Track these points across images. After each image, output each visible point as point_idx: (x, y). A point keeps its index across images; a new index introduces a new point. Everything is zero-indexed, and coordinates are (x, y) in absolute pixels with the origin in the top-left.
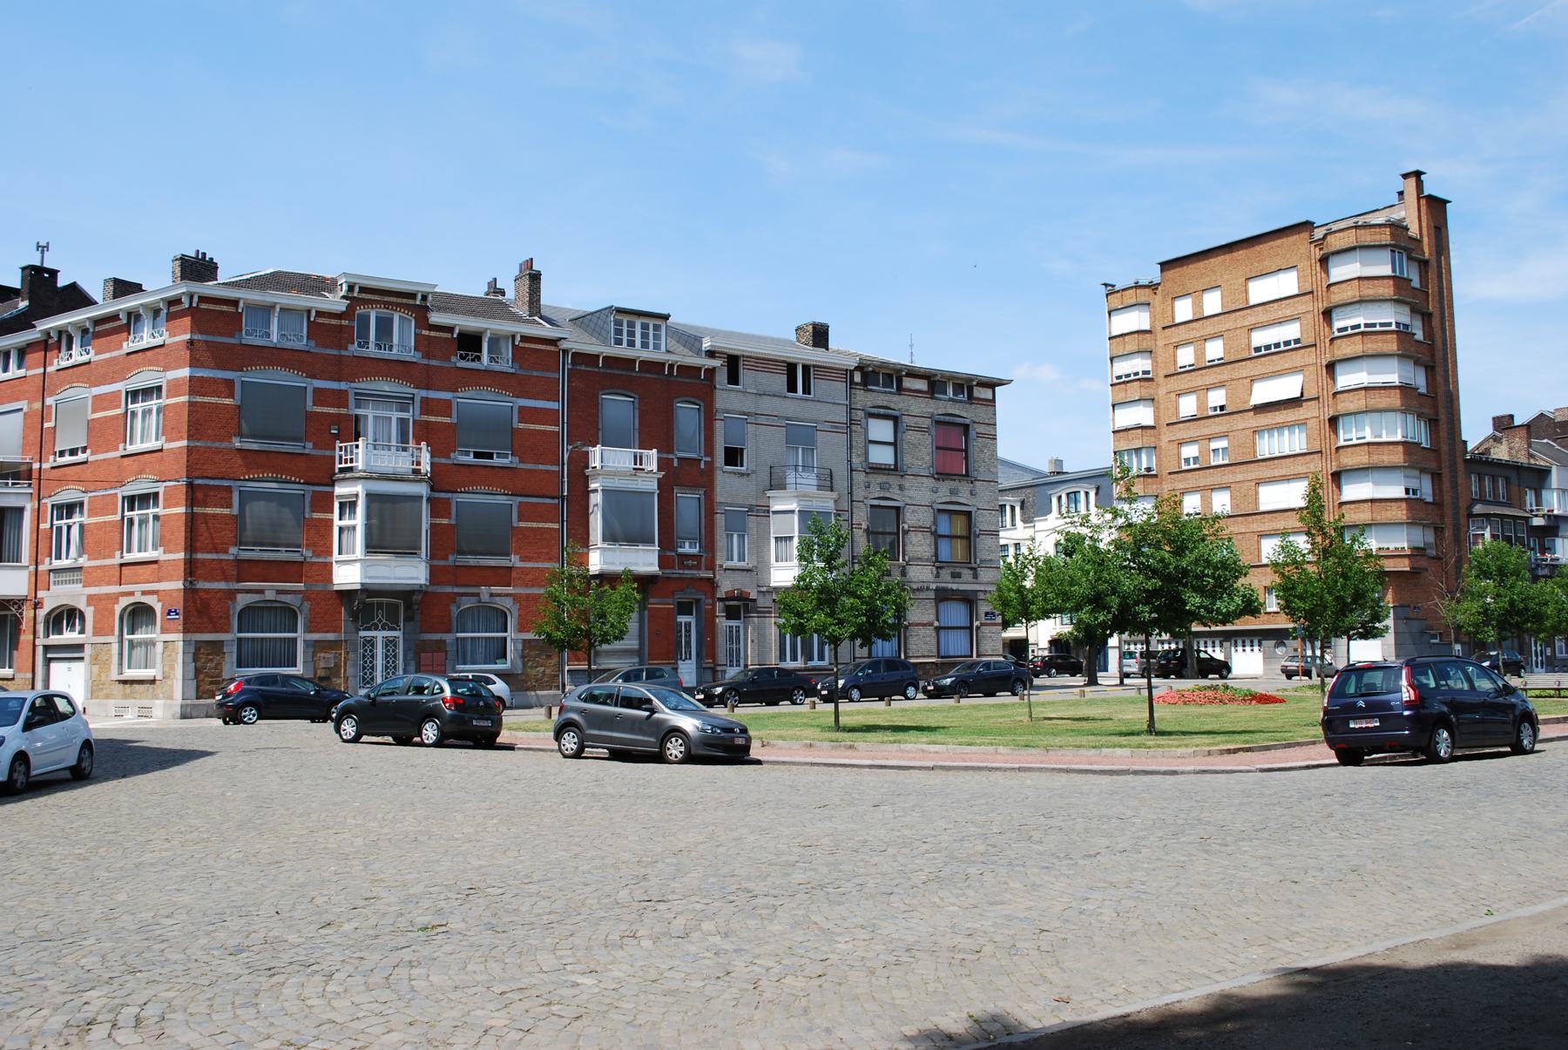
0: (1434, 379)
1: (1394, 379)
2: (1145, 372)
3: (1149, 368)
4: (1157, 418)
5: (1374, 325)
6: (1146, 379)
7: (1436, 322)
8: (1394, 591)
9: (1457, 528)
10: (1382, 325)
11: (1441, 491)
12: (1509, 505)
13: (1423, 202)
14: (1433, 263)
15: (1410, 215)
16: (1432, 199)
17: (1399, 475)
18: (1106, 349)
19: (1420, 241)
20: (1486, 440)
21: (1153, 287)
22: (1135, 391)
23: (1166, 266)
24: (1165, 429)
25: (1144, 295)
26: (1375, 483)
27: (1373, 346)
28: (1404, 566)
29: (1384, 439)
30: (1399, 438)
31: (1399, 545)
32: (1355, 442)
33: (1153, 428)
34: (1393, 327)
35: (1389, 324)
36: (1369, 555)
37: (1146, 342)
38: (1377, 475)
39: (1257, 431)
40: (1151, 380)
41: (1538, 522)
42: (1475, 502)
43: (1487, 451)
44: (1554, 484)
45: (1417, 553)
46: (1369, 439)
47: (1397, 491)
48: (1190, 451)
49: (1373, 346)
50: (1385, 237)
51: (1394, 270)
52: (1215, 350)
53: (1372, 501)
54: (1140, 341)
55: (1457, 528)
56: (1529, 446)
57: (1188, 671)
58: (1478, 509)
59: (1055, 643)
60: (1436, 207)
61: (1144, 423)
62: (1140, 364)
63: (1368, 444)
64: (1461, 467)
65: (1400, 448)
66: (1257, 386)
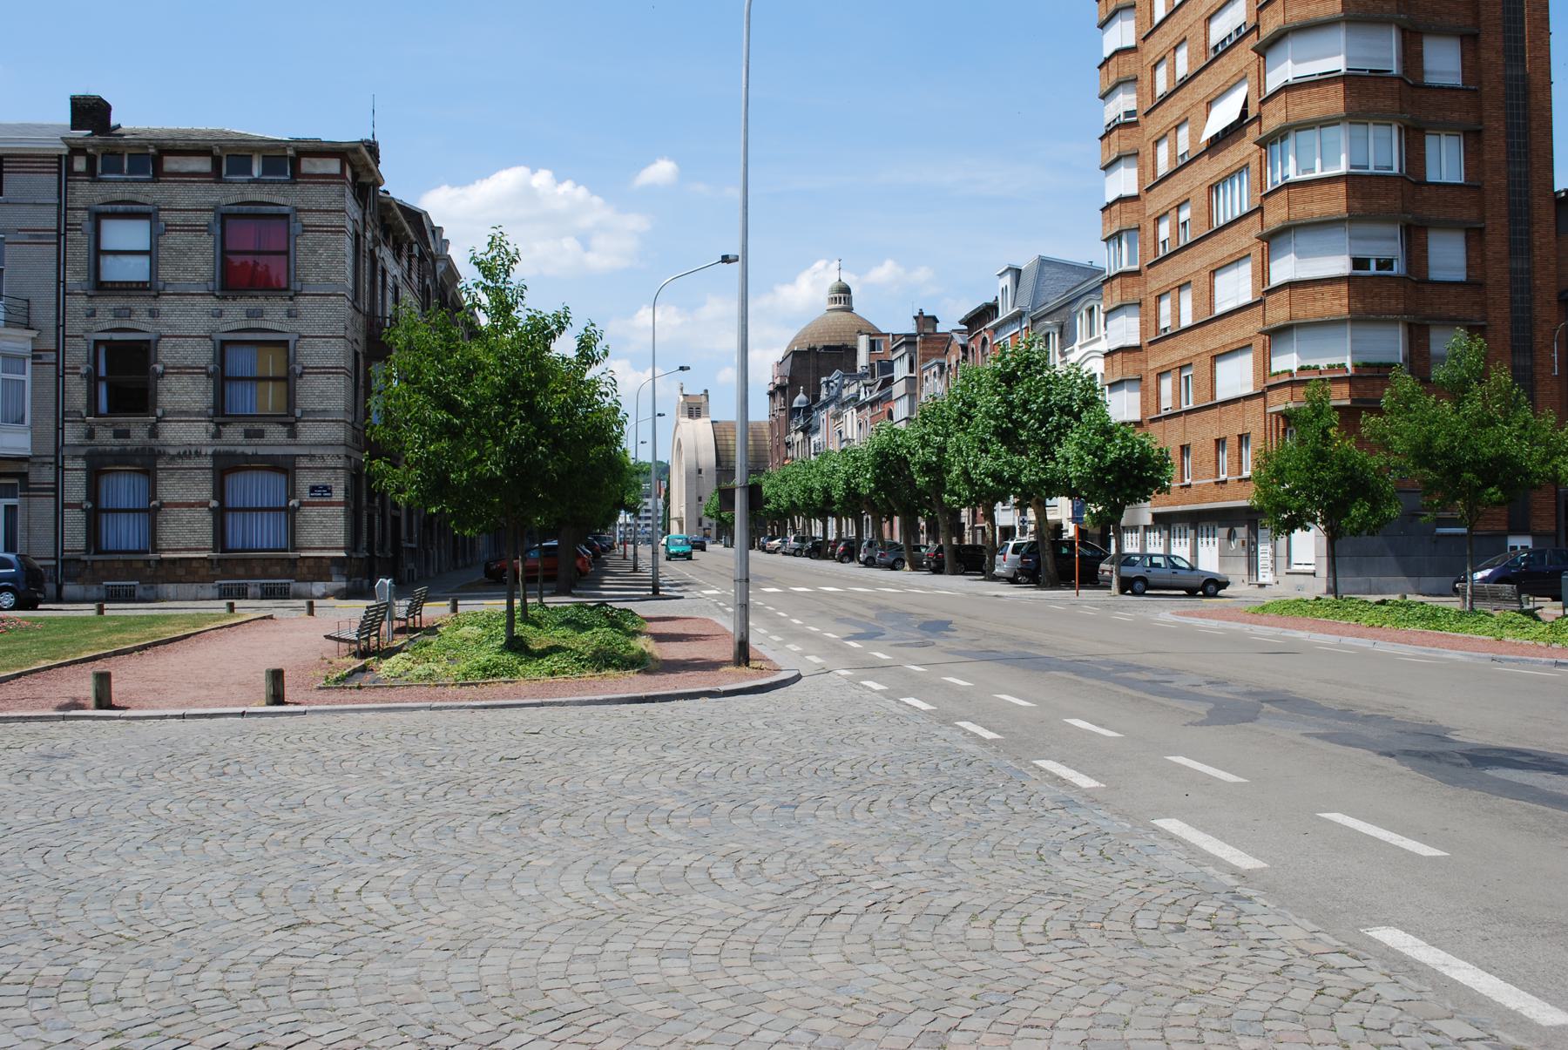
1: (1338, 63)
2: (1128, 114)
3: (1132, 107)
6: (1128, 123)
17: (1341, 237)
18: (1096, 82)
22: (1118, 143)
26: (1301, 255)
29: (1318, 173)
30: (1343, 168)
31: (1335, 361)
37: (1128, 66)
38: (1301, 240)
39: (1214, 187)
40: (1135, 124)
45: (1370, 375)
47: (1339, 265)
48: (1165, 230)
54: (1120, 71)
62: (1124, 102)
63: (1289, 186)
64: (1544, 214)
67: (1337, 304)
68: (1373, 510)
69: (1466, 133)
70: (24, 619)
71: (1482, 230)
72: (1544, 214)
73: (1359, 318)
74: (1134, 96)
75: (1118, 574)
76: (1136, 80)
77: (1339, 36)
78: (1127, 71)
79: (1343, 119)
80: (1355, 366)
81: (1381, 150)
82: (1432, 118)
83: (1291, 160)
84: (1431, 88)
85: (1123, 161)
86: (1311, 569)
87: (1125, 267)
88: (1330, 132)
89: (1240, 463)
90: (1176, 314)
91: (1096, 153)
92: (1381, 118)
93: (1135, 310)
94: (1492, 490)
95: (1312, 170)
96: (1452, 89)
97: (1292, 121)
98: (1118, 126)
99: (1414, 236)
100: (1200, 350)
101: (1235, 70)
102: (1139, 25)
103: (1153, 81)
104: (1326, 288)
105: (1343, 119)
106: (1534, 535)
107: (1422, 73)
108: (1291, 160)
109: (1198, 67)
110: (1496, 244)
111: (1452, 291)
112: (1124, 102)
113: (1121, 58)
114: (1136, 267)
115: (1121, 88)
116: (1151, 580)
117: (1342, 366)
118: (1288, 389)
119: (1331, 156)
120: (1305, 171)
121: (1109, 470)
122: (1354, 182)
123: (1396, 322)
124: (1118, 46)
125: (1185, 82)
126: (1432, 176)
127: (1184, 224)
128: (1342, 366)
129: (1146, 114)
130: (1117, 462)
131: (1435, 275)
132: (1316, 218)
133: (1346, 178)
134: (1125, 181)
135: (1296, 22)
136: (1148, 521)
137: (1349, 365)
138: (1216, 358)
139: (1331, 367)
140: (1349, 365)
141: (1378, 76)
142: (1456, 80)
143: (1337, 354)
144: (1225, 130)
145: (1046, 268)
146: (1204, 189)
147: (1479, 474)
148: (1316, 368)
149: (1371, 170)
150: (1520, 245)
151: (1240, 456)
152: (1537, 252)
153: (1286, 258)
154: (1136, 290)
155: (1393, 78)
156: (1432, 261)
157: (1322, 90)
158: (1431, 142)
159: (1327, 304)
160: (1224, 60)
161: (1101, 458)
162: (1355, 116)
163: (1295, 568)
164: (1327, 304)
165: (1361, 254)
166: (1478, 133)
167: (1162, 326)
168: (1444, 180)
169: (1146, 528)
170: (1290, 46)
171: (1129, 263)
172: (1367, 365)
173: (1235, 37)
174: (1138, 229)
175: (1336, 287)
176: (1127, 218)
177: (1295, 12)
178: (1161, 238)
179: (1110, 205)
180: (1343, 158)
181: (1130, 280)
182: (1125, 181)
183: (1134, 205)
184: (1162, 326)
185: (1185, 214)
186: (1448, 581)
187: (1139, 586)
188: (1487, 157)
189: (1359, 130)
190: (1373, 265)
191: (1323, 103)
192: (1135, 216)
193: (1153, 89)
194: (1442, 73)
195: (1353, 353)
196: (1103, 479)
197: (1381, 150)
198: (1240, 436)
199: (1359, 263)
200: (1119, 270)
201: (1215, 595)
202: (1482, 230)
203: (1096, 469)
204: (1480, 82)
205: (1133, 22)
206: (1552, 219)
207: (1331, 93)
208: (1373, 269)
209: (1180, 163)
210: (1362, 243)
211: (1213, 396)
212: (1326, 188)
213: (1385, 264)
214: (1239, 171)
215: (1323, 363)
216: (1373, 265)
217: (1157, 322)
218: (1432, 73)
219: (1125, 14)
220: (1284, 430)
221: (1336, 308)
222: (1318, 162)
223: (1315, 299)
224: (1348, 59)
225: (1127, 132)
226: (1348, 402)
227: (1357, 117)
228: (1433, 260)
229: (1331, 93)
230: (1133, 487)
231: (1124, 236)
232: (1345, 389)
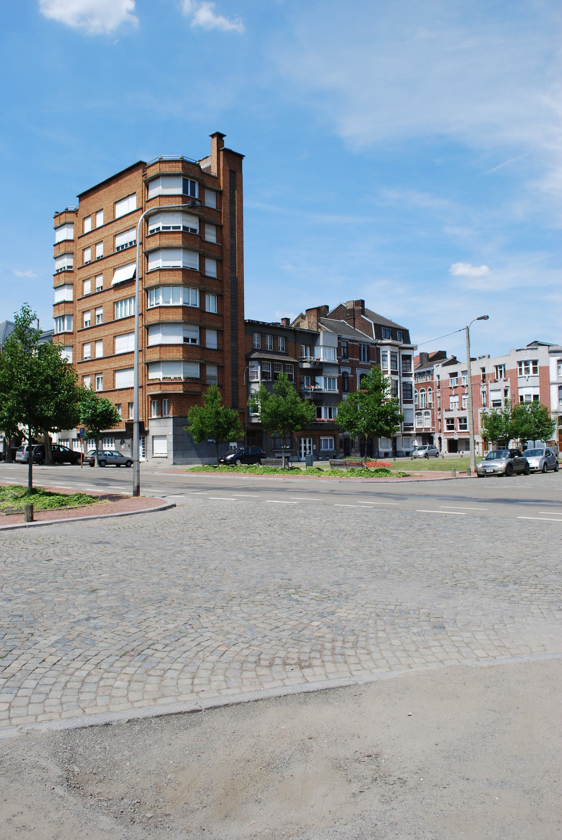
0: (222, 269)
1: (180, 264)
2: (69, 267)
3: (71, 264)
4: (74, 296)
5: (169, 228)
6: (68, 271)
7: (226, 232)
8: (174, 406)
9: (235, 366)
10: (174, 228)
11: (223, 341)
12: (286, 354)
13: (222, 153)
14: (227, 193)
15: (210, 163)
16: (229, 153)
17: (180, 329)
18: (52, 252)
19: (217, 178)
20: (298, 318)
21: (76, 212)
22: (63, 279)
23: (82, 196)
24: (77, 302)
25: (70, 217)
26: (164, 334)
27: (166, 241)
28: (179, 390)
29: (171, 304)
30: (181, 303)
31: (177, 376)
32: (155, 306)
33: (71, 302)
34: (181, 229)
35: (179, 228)
36: (305, 389)
37: (70, 247)
38: (165, 329)
39: (116, 303)
40: (72, 272)
41: (306, 366)
42: (254, 351)
43: (298, 325)
44: (321, 343)
45: (189, 381)
46: (161, 304)
47: (179, 340)
48: (87, 317)
49: (166, 241)
50: (178, 168)
51: (185, 190)
52: (100, 251)
53: (161, 346)
54: (65, 248)
55: (235, 366)
56: (319, 320)
57: (46, 460)
58: (255, 355)
59: (51, 439)
60: (233, 161)
61: (66, 300)
62: (66, 262)
63: (160, 307)
64: (241, 327)
65: (181, 310)
66: (117, 273)
67: (178, 354)
68: (237, 433)
69: (218, 295)
70: (145, 508)
71: (223, 331)
72: (241, 327)
73: (187, 360)
74: (72, 260)
75: (97, 458)
76: (73, 253)
77: (180, 253)
78: (69, 250)
79: (181, 285)
80: (184, 378)
81: (192, 298)
82: (208, 289)
83: (161, 297)
84: (208, 277)
85: (66, 286)
86: (165, 455)
87: (66, 330)
88: (176, 289)
89: (129, 414)
90: (93, 351)
91: (52, 282)
92: (194, 287)
93: (71, 349)
94: (297, 426)
95: (169, 302)
96: (214, 279)
97: (162, 282)
98: (64, 271)
99: (202, 330)
100: (107, 367)
101: (129, 258)
102: (76, 232)
103: (83, 255)
104: (174, 348)
105: (181, 285)
106: (237, 442)
107: (205, 271)
108: (161, 297)
109: (109, 254)
110: (227, 336)
111: (213, 352)
112: (66, 262)
113: (67, 244)
114: (71, 331)
115: (66, 256)
116: (108, 461)
117: (180, 378)
118: (159, 386)
119: (178, 298)
120: (166, 303)
121: (98, 416)
122: (185, 309)
123: (197, 362)
124: (65, 238)
125: (100, 259)
126: (207, 310)
127: (98, 316)
128: (180, 378)
129: (79, 269)
130: (100, 413)
131: (208, 346)
132: (171, 321)
133: (182, 307)
134: (66, 294)
135: (164, 245)
136: (75, 437)
137: (182, 378)
138: (115, 371)
139: (175, 378)
140: (182, 378)
141: (192, 270)
142: (215, 276)
143: (178, 373)
144: (122, 282)
145: (9, 326)
146: (111, 303)
147: (294, 421)
148: (170, 378)
149: (190, 305)
150: (235, 338)
151: (129, 411)
152: (239, 341)
153: (158, 335)
154: (71, 340)
155: (198, 272)
156: (207, 341)
157: (174, 273)
158: (207, 296)
159: (174, 354)
160: (124, 253)
161: (95, 411)
162: (186, 284)
163: (155, 455)
164: (174, 354)
165: (187, 336)
166: (222, 296)
167: (85, 356)
168: (211, 312)
169: (74, 440)
170: (161, 254)
171: (68, 329)
172: (188, 378)
173: (129, 246)
174: (73, 315)
175: (178, 348)
176: (68, 310)
177: (164, 241)
178: (85, 320)
179: (58, 304)
180: (181, 299)
181: (68, 336)
182: (66, 294)
183: (71, 305)
184: (85, 356)
185: (99, 312)
186: (216, 459)
187: (103, 463)
188: (225, 305)
189: (186, 289)
190: (190, 340)
191: (174, 278)
192: (71, 310)
193: (83, 259)
194: (210, 272)
195: (184, 373)
196: (95, 419)
197: (192, 298)
198: (129, 403)
199: (186, 340)
200: (62, 331)
201: (130, 467)
202: (223, 331)
203: (93, 415)
204: (223, 278)
205: (73, 229)
206: (244, 329)
207: (177, 274)
208: (190, 343)
209: (97, 291)
210: (187, 332)
211: (114, 387)
212: (175, 310)
213: (194, 340)
214: (130, 298)
215: (172, 377)
216: (190, 340)
217: (82, 354)
218: (208, 272)
219: (69, 226)
220: (151, 401)
221: (178, 356)
222: (171, 300)
223: (170, 352)
224: (183, 263)
225: (69, 274)
226: (182, 392)
227: (187, 285)
228: (208, 341)
229: (177, 274)
230: (106, 422)
231: (66, 318)
232: (181, 387)
